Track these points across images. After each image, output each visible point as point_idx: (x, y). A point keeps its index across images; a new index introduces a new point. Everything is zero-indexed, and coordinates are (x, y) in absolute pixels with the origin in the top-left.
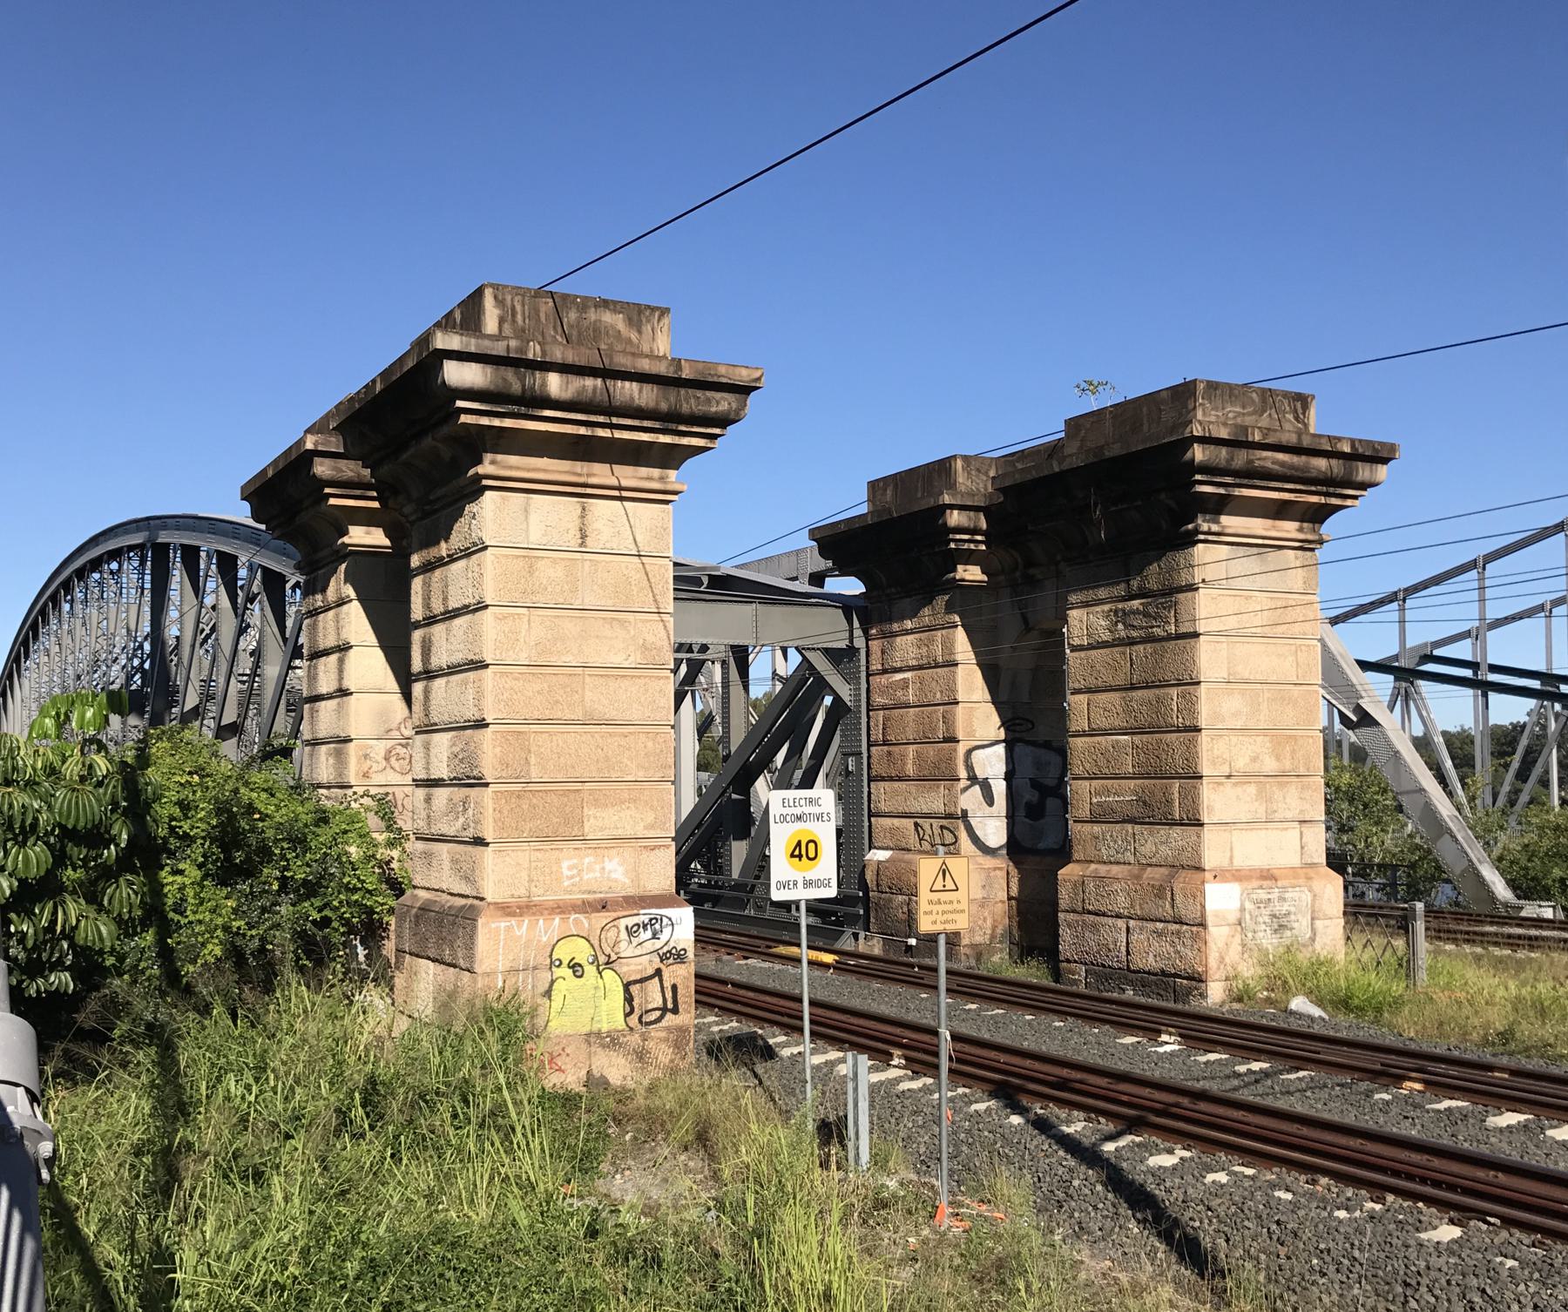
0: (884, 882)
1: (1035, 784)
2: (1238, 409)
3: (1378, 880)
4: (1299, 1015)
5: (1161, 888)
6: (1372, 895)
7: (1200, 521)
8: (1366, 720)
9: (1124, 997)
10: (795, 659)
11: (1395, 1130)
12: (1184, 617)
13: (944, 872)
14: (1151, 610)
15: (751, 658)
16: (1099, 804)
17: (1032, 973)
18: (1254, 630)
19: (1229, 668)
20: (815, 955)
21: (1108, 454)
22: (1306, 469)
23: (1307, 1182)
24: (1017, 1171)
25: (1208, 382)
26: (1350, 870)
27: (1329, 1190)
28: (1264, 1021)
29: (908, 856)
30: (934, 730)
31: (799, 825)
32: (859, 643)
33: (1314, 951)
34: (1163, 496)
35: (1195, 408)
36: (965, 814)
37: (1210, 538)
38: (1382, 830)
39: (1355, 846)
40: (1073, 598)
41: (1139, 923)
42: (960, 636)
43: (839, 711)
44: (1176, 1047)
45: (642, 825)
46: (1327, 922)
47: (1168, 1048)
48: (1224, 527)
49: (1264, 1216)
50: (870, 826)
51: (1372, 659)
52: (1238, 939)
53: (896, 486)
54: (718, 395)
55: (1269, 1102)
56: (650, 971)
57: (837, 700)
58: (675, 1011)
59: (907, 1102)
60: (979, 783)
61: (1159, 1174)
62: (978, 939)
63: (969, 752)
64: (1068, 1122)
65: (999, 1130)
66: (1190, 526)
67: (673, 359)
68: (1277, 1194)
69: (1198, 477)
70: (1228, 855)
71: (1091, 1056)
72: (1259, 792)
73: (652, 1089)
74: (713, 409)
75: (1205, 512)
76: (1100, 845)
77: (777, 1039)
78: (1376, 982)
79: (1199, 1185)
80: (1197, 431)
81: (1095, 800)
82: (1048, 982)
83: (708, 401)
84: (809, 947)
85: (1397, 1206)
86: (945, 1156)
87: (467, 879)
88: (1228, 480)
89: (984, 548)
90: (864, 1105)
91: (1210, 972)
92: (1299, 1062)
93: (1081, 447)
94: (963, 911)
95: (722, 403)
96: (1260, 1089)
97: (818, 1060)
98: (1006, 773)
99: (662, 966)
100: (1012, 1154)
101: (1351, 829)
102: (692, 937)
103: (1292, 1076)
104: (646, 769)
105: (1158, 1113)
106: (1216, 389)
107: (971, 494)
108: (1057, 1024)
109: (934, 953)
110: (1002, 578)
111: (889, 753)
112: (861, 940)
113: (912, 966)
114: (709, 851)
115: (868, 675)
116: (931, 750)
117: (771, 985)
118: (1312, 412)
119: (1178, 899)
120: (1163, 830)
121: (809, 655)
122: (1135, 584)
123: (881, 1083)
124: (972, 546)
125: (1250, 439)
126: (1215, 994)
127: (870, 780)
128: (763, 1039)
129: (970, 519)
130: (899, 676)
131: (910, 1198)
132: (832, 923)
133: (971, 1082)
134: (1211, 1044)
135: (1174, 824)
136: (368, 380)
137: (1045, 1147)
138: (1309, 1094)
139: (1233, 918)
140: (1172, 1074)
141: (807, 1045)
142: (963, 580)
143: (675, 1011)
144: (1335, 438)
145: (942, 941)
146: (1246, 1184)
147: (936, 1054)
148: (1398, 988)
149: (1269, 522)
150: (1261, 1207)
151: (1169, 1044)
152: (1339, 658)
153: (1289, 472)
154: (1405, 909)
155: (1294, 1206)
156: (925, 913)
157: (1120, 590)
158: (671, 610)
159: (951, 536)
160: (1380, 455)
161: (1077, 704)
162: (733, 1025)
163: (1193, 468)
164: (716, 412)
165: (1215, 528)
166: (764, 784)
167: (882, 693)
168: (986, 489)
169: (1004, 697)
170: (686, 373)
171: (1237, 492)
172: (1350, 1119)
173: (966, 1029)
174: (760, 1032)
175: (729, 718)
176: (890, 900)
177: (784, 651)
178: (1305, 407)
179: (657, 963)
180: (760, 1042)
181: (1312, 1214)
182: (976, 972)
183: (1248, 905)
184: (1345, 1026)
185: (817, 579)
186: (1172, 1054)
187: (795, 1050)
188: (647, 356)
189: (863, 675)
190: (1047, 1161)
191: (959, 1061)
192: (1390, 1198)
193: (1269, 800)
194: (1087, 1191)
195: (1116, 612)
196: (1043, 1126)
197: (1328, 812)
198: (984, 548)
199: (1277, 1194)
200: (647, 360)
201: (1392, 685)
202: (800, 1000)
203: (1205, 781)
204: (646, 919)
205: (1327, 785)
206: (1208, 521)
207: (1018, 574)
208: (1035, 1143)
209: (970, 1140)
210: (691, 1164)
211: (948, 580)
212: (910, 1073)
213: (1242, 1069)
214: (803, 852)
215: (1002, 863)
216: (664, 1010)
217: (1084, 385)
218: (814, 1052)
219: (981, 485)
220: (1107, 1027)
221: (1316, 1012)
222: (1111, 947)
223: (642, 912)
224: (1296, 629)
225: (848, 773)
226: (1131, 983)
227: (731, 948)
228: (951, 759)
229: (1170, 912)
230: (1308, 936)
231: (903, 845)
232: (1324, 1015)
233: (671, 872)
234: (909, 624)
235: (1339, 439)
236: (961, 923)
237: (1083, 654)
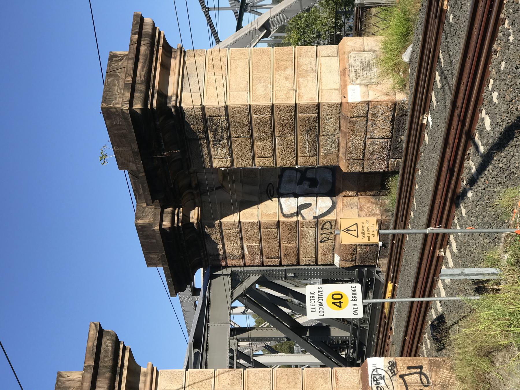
0: (350, 257)
1: (300, 183)
2: (116, 88)
3: (343, 20)
4: (411, 58)
5: (351, 122)
6: (351, 23)
7: (170, 105)
8: (266, 26)
9: (405, 141)
10: (237, 303)
11: (468, 13)
12: (217, 112)
13: (348, 230)
14: (214, 127)
15: (236, 326)
16: (310, 152)
17: (394, 184)
18: (224, 79)
19: (242, 91)
20: (389, 294)
21: (136, 149)
22: (146, 55)
23: (496, 54)
24: (496, 194)
25: (102, 102)
26: (338, 33)
27: (499, 44)
28: (415, 74)
29: (337, 246)
30: (273, 233)
31: (325, 303)
32: (229, 271)
33: (379, 50)
34: (158, 123)
35: (115, 108)
36: (316, 218)
37: (179, 100)
38: (319, 18)
39: (327, 31)
40: (208, 165)
41: (368, 133)
42: (225, 220)
43: (263, 281)
44: (429, 116)
45: (325, 385)
46: (366, 44)
47: (430, 120)
48: (173, 94)
49: (514, 75)
50: (323, 265)
51: (236, 23)
52: (374, 86)
53: (150, 253)
54: (103, 346)
55: (456, 73)
56: (401, 381)
57: (258, 282)
58: (421, 367)
59: (463, 248)
60: (300, 211)
61: (495, 125)
62: (378, 211)
63: (284, 215)
64: (470, 169)
65: (475, 202)
66: (173, 110)
67: (84, 370)
68: (502, 69)
69: (149, 106)
70: (333, 91)
71: (436, 157)
72: (303, 76)
73: (462, 380)
74: (110, 348)
75: (166, 103)
76: (330, 152)
77: (433, 314)
78: (394, 21)
79: (499, 106)
80: (126, 107)
81: (308, 154)
82: (399, 177)
83: (106, 351)
84: (384, 298)
85: (506, 13)
86: (491, 230)
88: (150, 92)
89: (181, 209)
90: (467, 271)
91: (391, 99)
92: (435, 58)
93: (133, 162)
94: (367, 221)
95: (107, 344)
96: (449, 76)
97: (443, 293)
98: (295, 197)
99: (398, 375)
100: (487, 197)
101: (319, 32)
102: (383, 358)
103: (442, 61)
104: (296, 383)
105: (463, 124)
106: (106, 98)
107: (155, 215)
108: (420, 173)
109: (386, 235)
110: (197, 200)
111: (285, 255)
112: (380, 269)
113: (393, 244)
114: (336, 348)
115: (245, 266)
116: (283, 234)
117: (405, 316)
118: (118, 53)
119: (356, 114)
120: (322, 122)
121: (235, 297)
122: (201, 136)
123: (454, 261)
124: (181, 215)
125: (131, 82)
126: (402, 97)
127: (299, 265)
128: (433, 321)
129: (167, 216)
130: (246, 251)
131: (513, 248)
132: (372, 284)
133: (451, 216)
134: (427, 100)
135: (319, 117)
137: (483, 180)
138: (451, 53)
139: (364, 89)
140: (443, 118)
141: (436, 298)
142: (198, 219)
143: (421, 367)
144: (131, 42)
145: (383, 231)
146: (498, 83)
147: (438, 234)
148: (397, 11)
149: (171, 73)
150: (509, 76)
151: (428, 119)
152: (236, 39)
153: (147, 64)
154: (357, 8)
155: (508, 60)
156: (369, 240)
157: (204, 143)
158: (213, 370)
159: (175, 225)
160: (140, 21)
161: (259, 163)
162: (427, 336)
163: (144, 109)
164: (112, 347)
165: (174, 98)
166: (300, 319)
167: (254, 259)
168: (152, 208)
169: (256, 199)
170: (92, 363)
171: (156, 88)
172: (463, 35)
173: (424, 218)
174: (430, 323)
175: (267, 338)
176: (360, 255)
177: (233, 308)
178: (116, 56)
179: (397, 377)
180: (436, 323)
181: (512, 52)
182: (395, 212)
183: (358, 81)
184: (416, 36)
185: (196, 292)
186: (433, 118)
187: (439, 304)
188: (82, 384)
189: (245, 269)
190: (490, 179)
191: (440, 223)
192: (502, 16)
193: (307, 72)
194: (505, 160)
195: (214, 145)
196: (472, 182)
197: (310, 44)
198: (181, 209)
199: (502, 69)
200: (85, 384)
201: (249, 14)
202: (412, 303)
203: (297, 102)
204: (374, 383)
205: (297, 44)
206: (171, 101)
207: (195, 192)
208: (481, 185)
209: (481, 217)
210: (500, 360)
211: (197, 227)
212: (448, 246)
213: (439, 85)
214: (338, 301)
215: (339, 199)
216: (421, 373)
217: (102, 161)
218: (439, 295)
219: (150, 210)
220: (420, 149)
221: (410, 49)
222: (380, 146)
223: (370, 385)
224: (224, 60)
225: (295, 276)
226: (398, 137)
227: (386, 336)
228: (288, 225)
229: (362, 118)
230: (372, 53)
231: (332, 248)
232: (411, 46)
233: (349, 369)
234: (220, 246)
235: (131, 40)
236: (373, 222)
237: (235, 160)
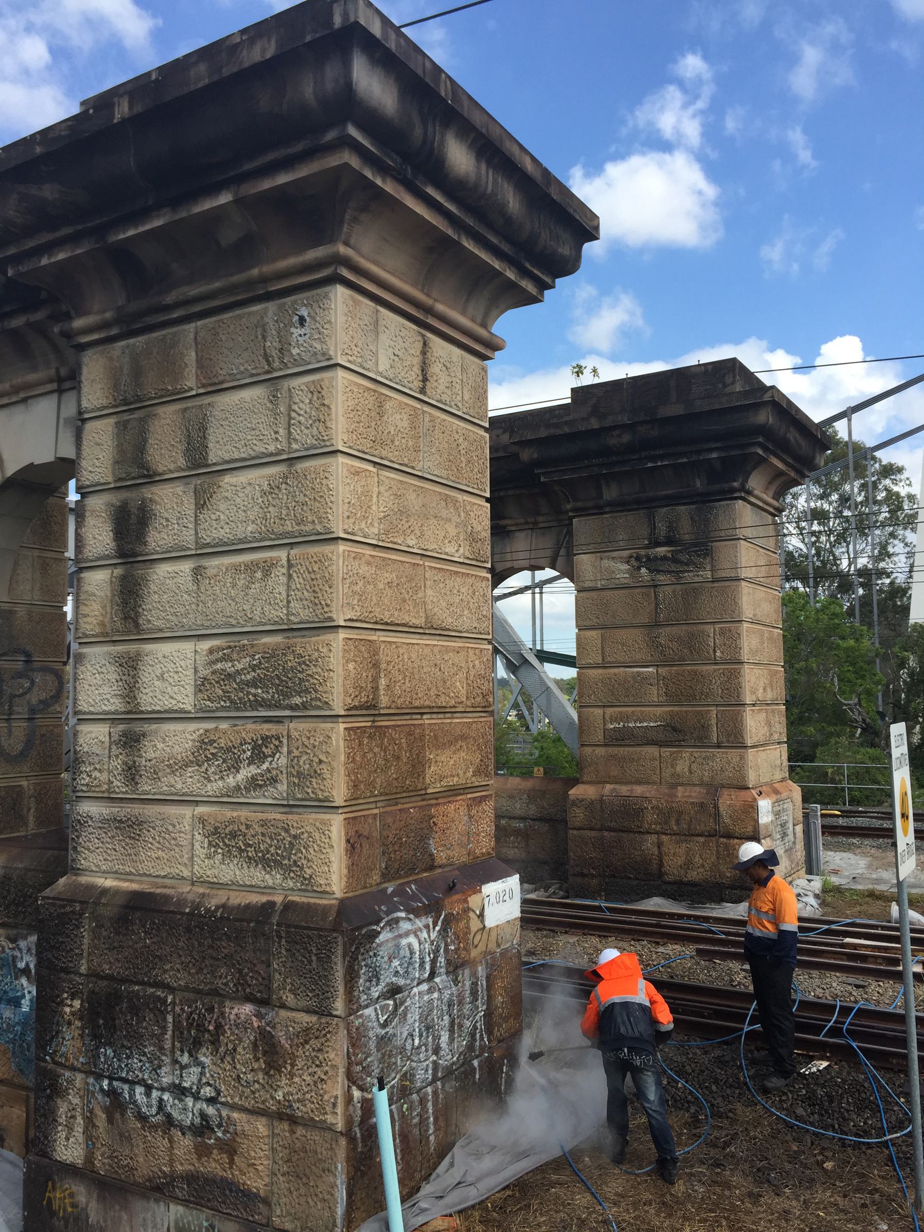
14: (684, 557)
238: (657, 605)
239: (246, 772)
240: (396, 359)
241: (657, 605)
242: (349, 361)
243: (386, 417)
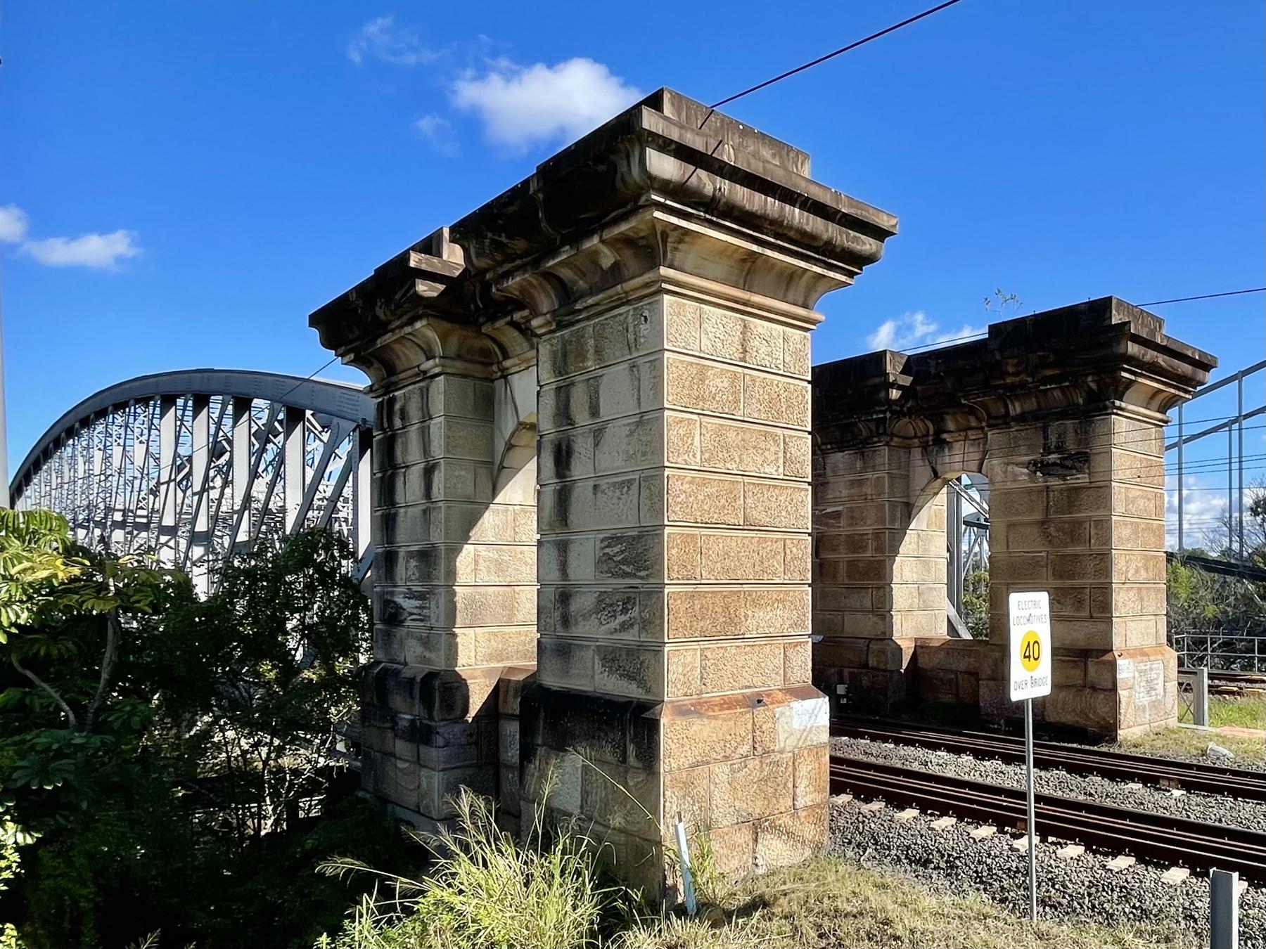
87: (631, 678)
95: (867, 244)
136: (516, 181)
171: (1140, 380)
238: (1048, 503)
239: (621, 618)
240: (717, 340)
241: (1048, 503)
242: (674, 346)
243: (707, 382)
